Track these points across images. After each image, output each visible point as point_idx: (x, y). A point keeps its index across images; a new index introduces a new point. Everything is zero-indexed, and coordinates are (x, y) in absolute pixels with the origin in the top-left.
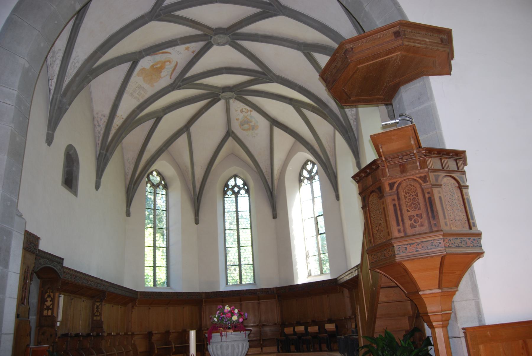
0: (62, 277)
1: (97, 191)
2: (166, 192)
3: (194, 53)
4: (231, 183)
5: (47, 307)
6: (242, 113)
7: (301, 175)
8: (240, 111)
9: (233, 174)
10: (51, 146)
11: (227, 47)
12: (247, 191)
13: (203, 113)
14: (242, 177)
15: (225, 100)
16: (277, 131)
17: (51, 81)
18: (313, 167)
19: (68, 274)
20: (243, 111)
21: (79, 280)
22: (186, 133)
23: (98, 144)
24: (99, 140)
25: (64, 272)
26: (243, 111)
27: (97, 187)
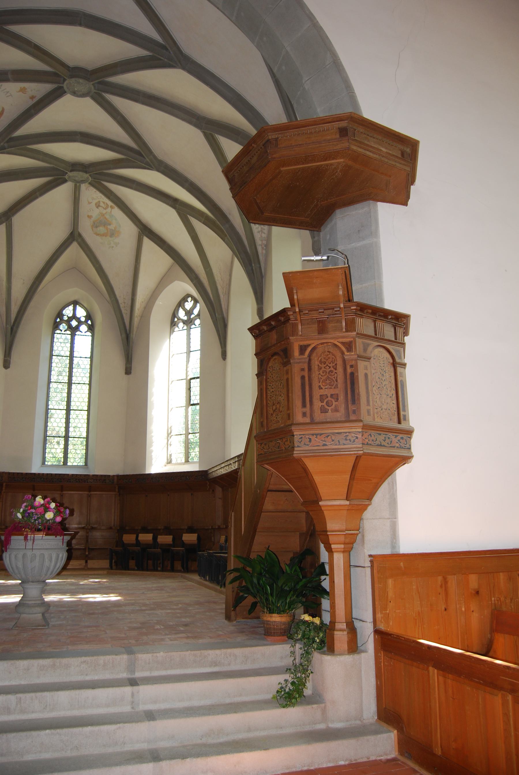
3: (34, 99)
4: (68, 312)
6: (97, 208)
7: (175, 315)
8: (96, 204)
9: (72, 299)
11: (88, 101)
12: (91, 328)
14: (85, 306)
15: (74, 183)
18: (194, 307)
20: (99, 206)
22: (4, 224)
26: (99, 206)
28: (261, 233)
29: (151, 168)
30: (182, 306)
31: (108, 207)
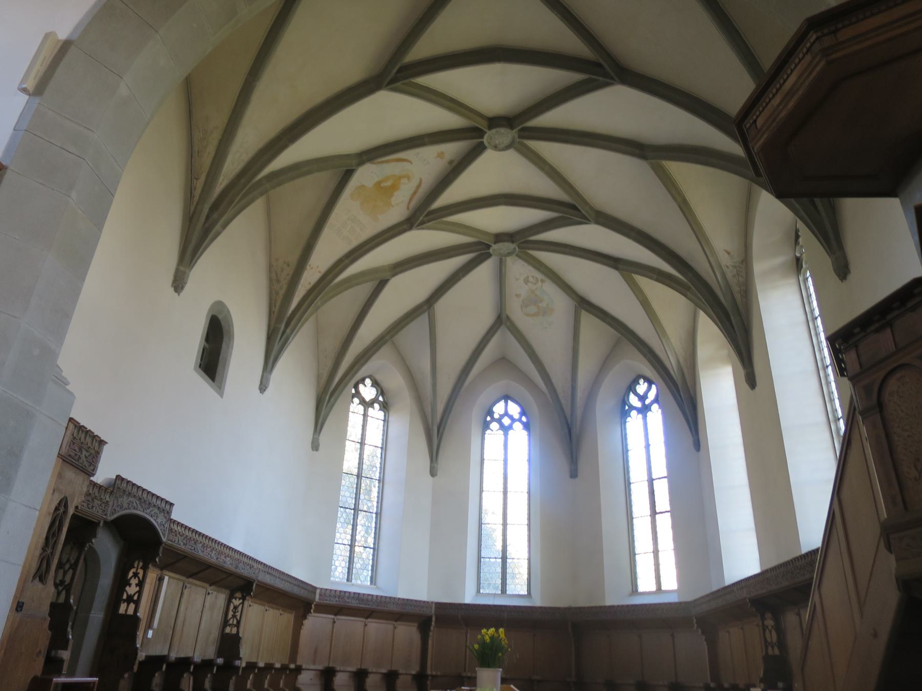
0: (164, 540)
1: (261, 394)
2: (385, 416)
4: (499, 409)
5: (128, 596)
6: (526, 284)
7: (624, 401)
8: (524, 280)
10: (181, 294)
11: (512, 154)
12: (526, 426)
13: (460, 279)
16: (587, 320)
17: (195, 181)
18: (649, 389)
19: (178, 535)
20: (528, 281)
21: (200, 551)
23: (274, 312)
24: (275, 306)
25: (171, 530)
26: (528, 281)
27: (263, 387)
28: (737, 277)
29: (585, 221)
30: (633, 390)
31: (538, 281)
